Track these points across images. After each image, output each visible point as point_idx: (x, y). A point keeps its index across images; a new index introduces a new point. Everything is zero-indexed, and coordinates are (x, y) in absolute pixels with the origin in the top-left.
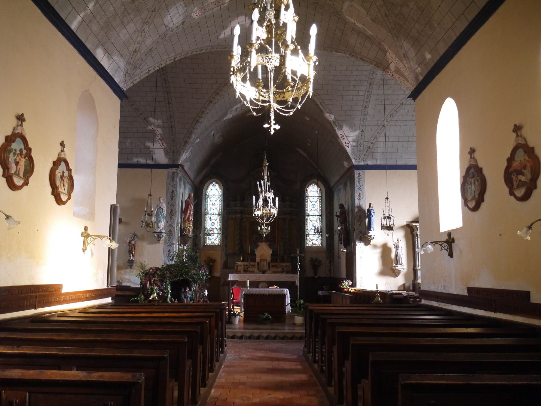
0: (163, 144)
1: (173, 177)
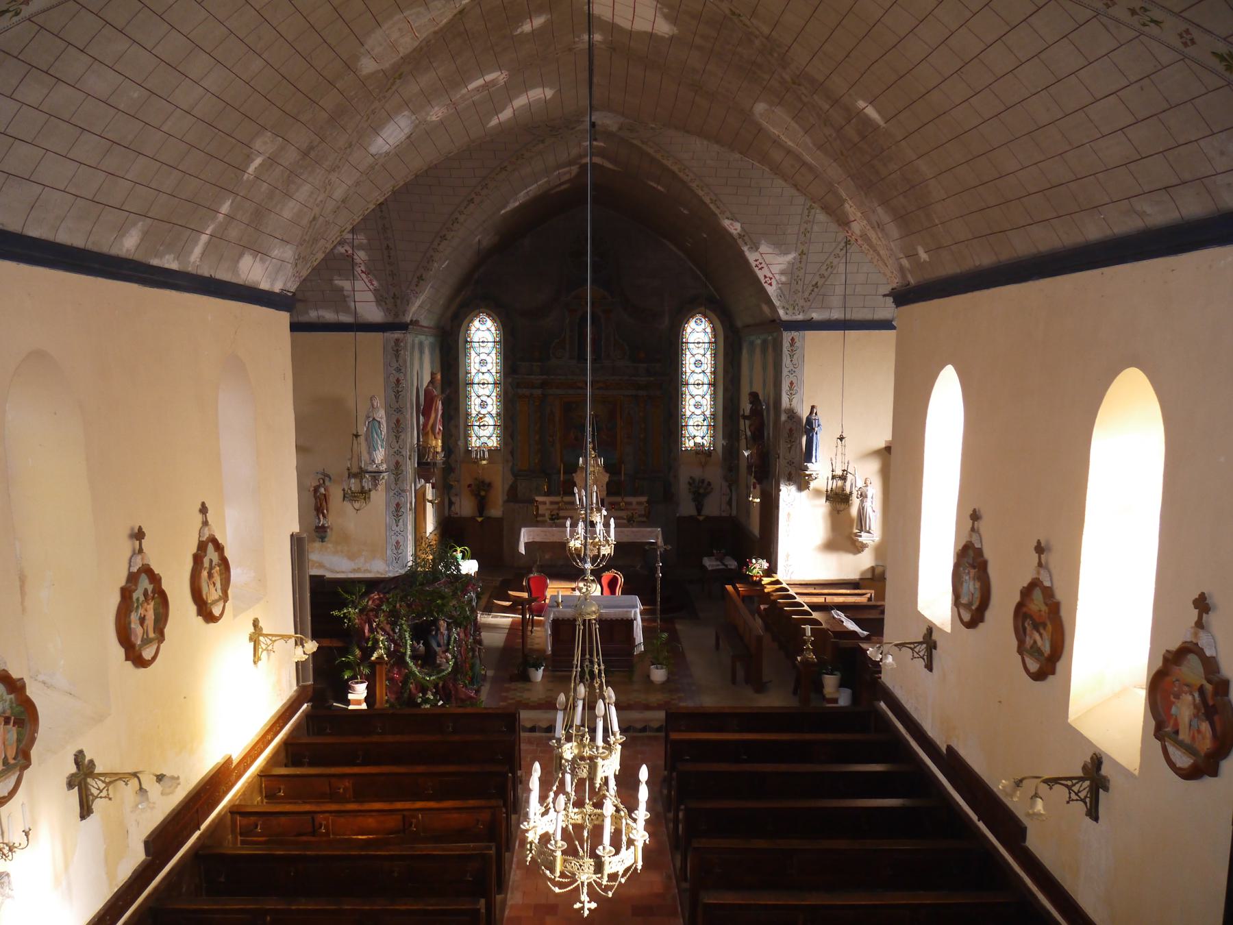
0: (371, 281)
1: (396, 349)
